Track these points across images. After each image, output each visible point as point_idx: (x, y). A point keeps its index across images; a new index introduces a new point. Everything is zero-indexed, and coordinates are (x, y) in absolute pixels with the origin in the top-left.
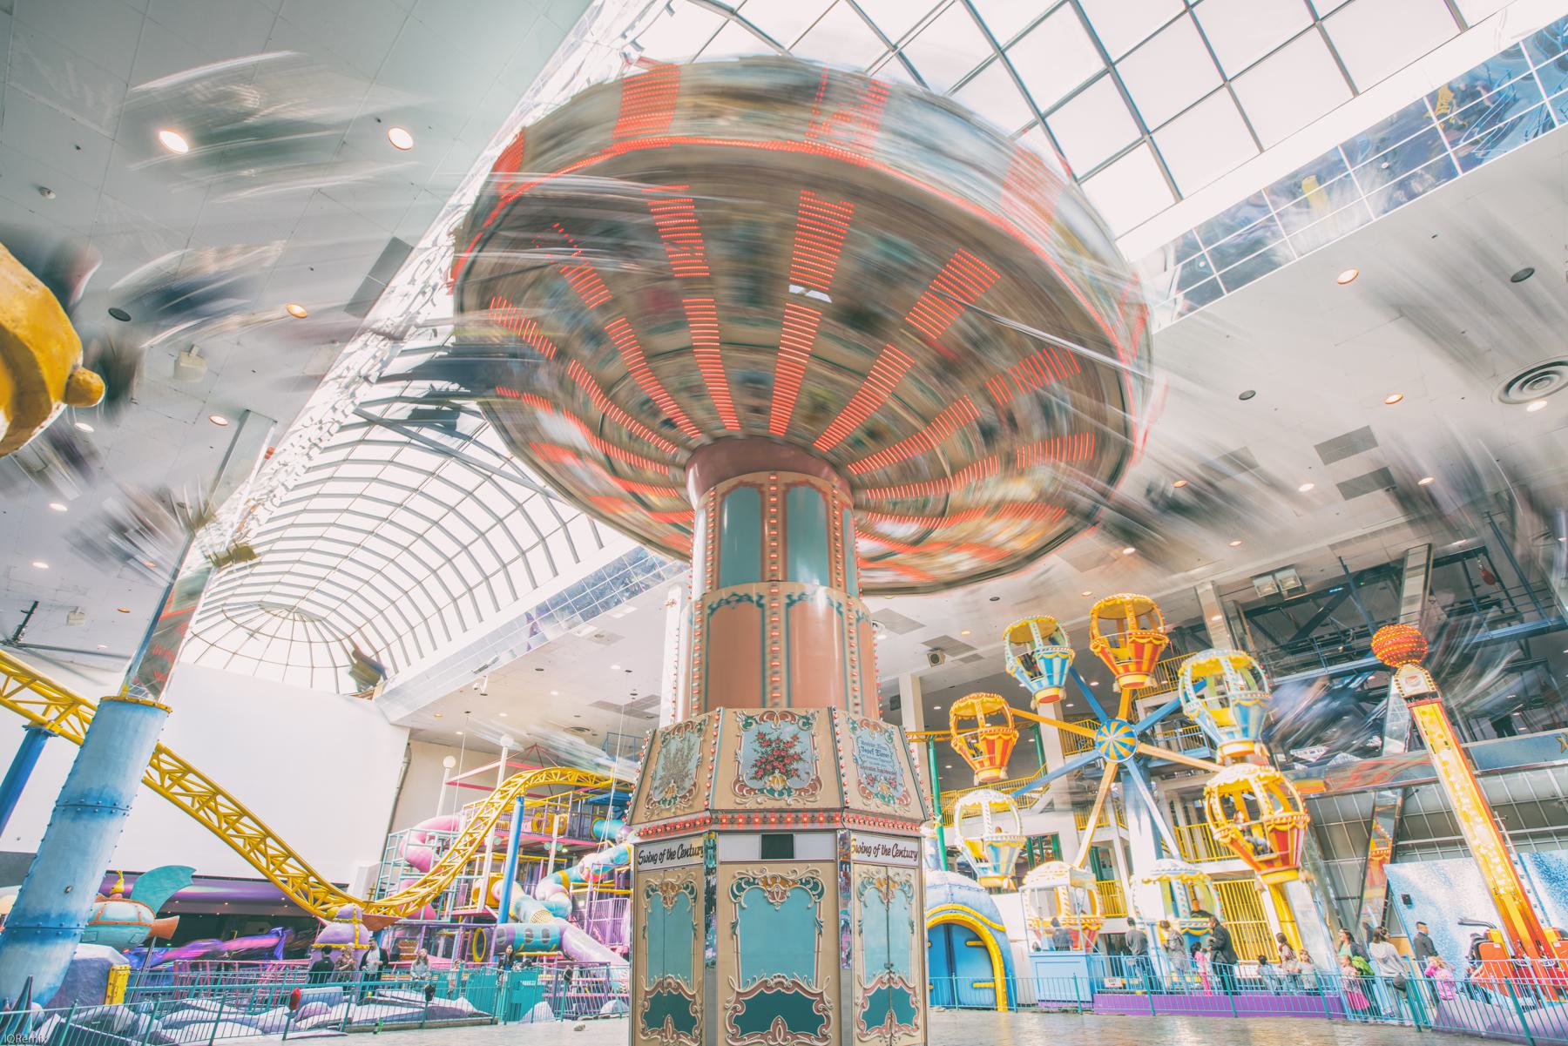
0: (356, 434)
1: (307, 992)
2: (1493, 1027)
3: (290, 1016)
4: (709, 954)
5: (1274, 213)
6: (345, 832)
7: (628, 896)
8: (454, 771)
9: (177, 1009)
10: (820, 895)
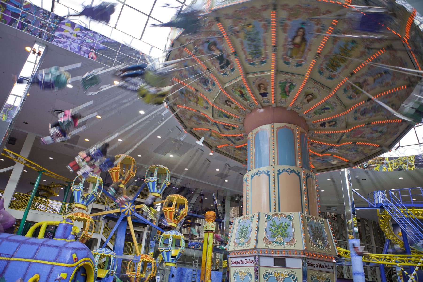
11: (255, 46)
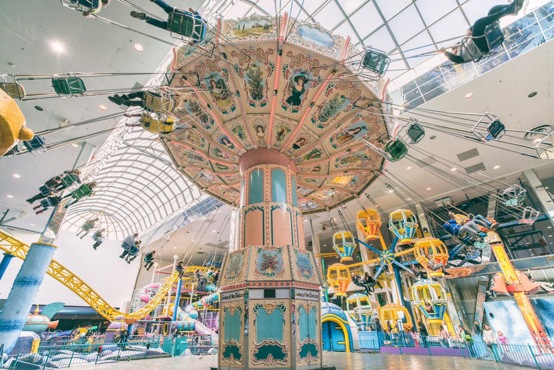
0: (124, 151)
1: (104, 346)
2: (524, 362)
3: (98, 355)
4: (246, 331)
5: (443, 74)
6: (118, 288)
7: (218, 311)
8: (158, 268)
9: (57, 354)
10: (285, 310)
11: (328, 112)
